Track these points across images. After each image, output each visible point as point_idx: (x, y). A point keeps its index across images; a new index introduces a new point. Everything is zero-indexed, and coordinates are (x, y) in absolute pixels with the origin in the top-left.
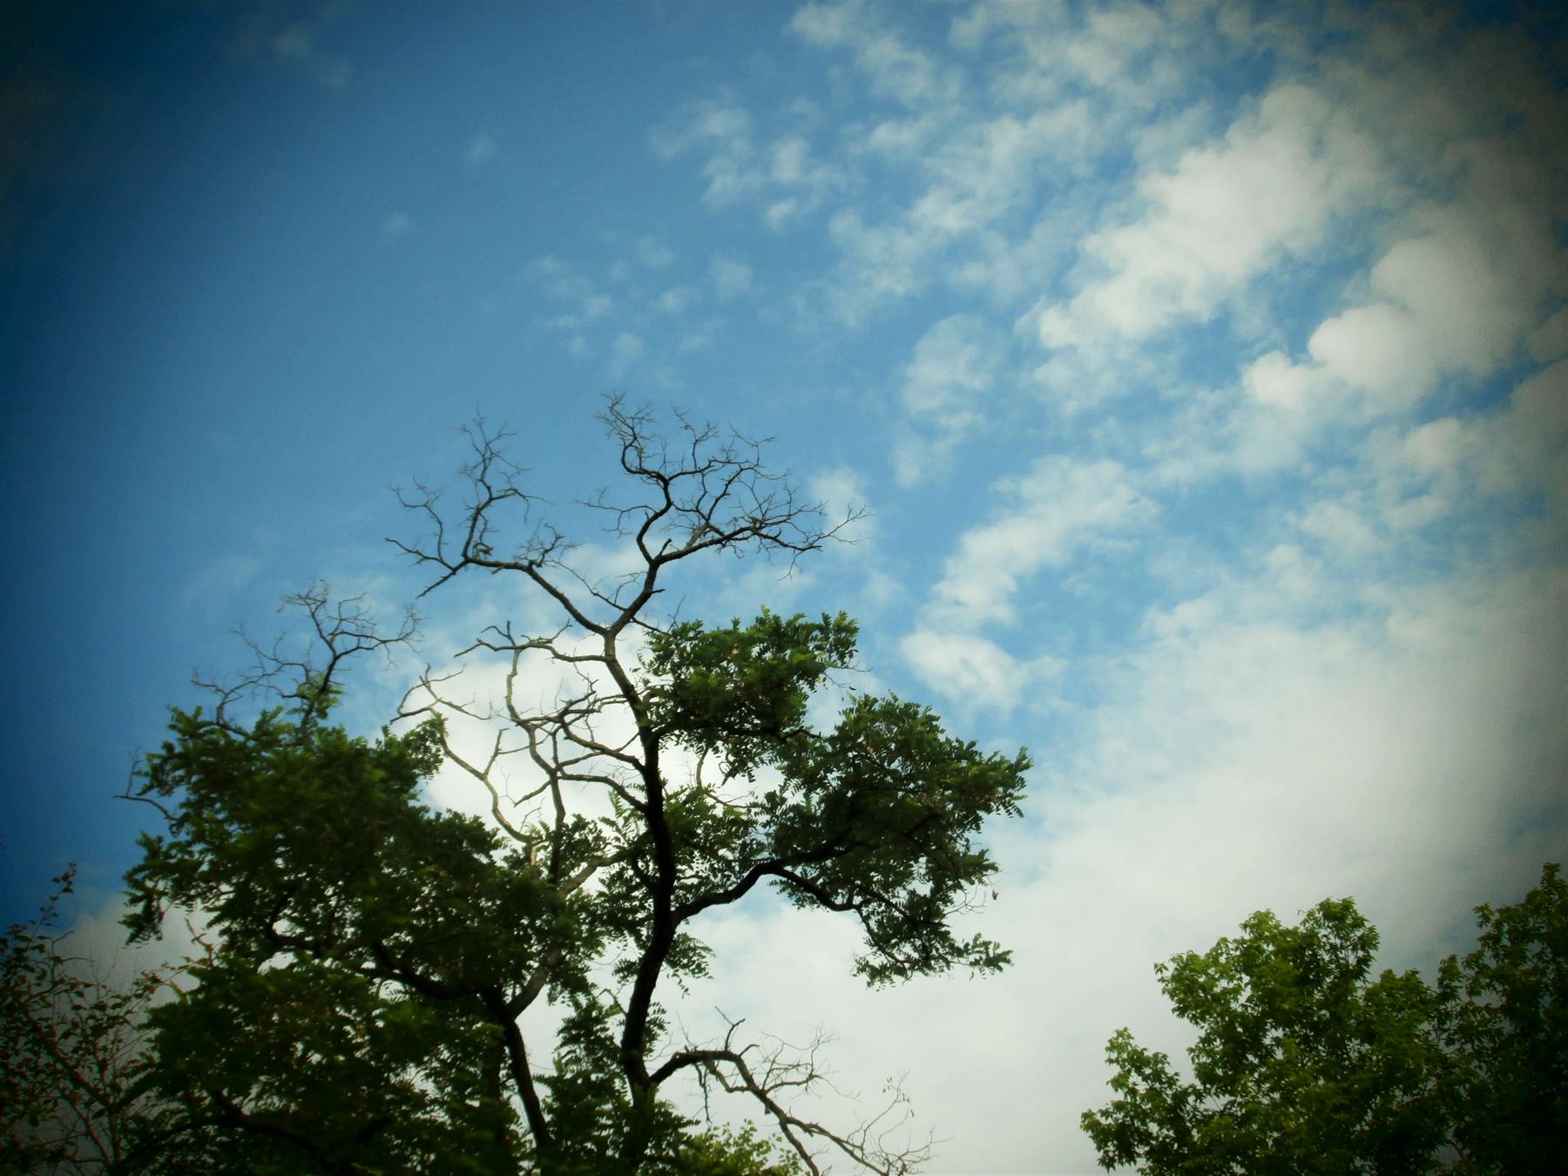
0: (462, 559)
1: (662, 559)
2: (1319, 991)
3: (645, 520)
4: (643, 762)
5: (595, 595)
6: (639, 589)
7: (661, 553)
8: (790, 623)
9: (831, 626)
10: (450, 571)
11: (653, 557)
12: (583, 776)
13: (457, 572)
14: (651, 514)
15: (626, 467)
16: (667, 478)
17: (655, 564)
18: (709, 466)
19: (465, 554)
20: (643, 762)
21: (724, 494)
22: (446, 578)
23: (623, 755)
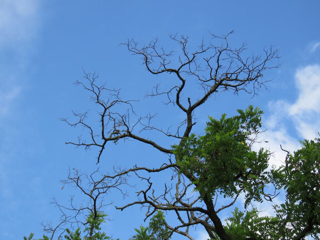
0: (104, 141)
1: (192, 109)
2: (250, 171)
3: (177, 92)
4: (205, 208)
5: (169, 136)
6: (186, 125)
7: (190, 106)
8: (222, 120)
9: (245, 115)
10: (102, 147)
11: (187, 108)
12: (129, 204)
13: (105, 146)
14: (178, 89)
15: (152, 73)
16: (177, 70)
17: (189, 112)
18: (194, 57)
19: (103, 138)
20: (205, 208)
21: (219, 67)
22: (101, 151)
23: (194, 208)
